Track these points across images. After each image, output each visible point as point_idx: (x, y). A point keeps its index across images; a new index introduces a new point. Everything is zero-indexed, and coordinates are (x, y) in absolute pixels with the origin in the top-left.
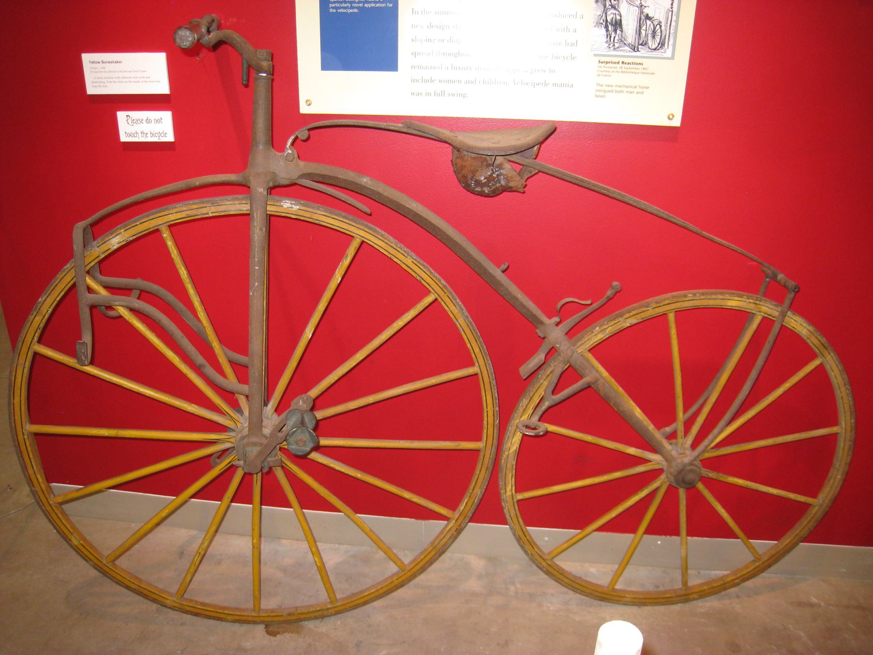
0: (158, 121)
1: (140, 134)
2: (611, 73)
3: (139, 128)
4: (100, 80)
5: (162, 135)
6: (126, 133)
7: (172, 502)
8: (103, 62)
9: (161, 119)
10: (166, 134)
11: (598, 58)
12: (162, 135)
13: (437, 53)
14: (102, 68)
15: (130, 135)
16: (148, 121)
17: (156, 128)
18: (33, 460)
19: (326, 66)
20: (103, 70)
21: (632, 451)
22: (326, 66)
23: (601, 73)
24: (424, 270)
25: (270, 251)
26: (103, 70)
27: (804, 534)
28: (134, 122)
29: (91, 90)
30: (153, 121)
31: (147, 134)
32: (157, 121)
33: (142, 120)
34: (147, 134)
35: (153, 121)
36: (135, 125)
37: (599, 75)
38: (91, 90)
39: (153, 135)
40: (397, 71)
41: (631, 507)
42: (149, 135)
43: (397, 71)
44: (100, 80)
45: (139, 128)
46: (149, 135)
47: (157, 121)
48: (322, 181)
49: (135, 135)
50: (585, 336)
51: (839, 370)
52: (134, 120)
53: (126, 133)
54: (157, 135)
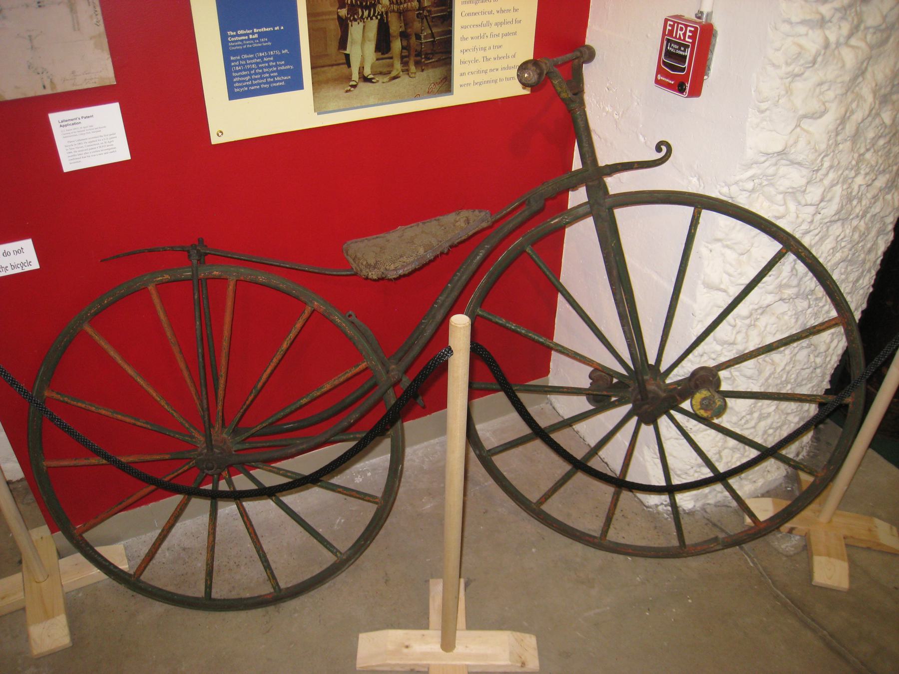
0: (20, 251)
2: (79, 160)
5: (26, 264)
9: (22, 249)
11: (114, 147)
12: (26, 264)
19: (233, 95)
22: (233, 95)
23: (72, 161)
25: (465, 540)
29: (68, 166)
30: (12, 253)
31: (7, 267)
32: (17, 252)
34: (7, 267)
35: (12, 253)
37: (71, 163)
38: (68, 166)
40: (230, 99)
42: (9, 268)
43: (230, 99)
46: (9, 268)
47: (17, 252)
50: (546, 183)
54: (19, 266)
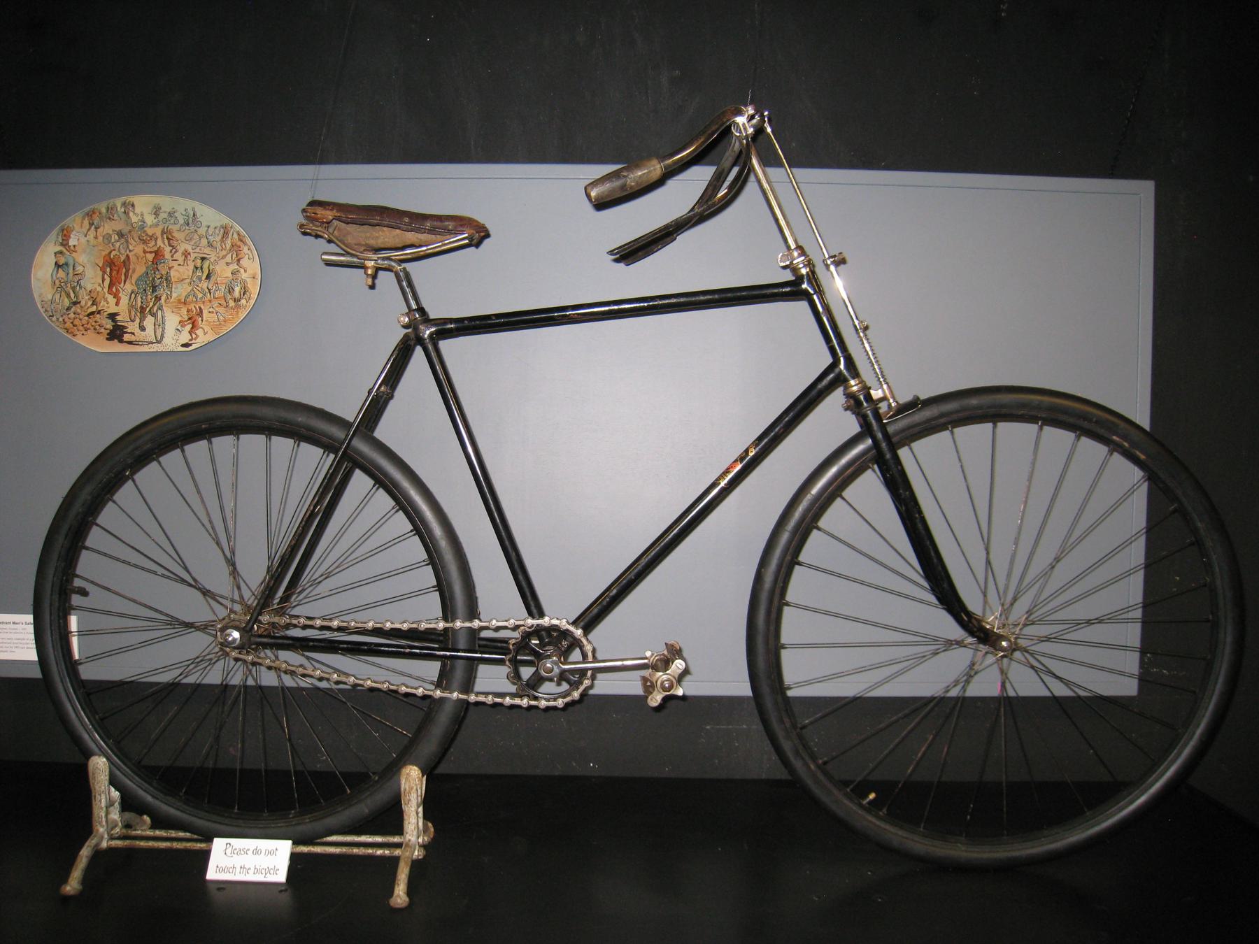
0: (271, 853)
3: (238, 861)
4: (9, 641)
5: (272, 872)
7: (278, 720)
8: (14, 623)
9: (276, 850)
14: (25, 629)
15: (223, 870)
16: (256, 852)
17: (264, 861)
18: (344, 850)
20: (23, 631)
26: (23, 631)
27: (389, 242)
28: (235, 852)
35: (263, 852)
36: (235, 856)
37: (675, 652)
39: (257, 871)
44: (9, 641)
45: (238, 861)
46: (251, 872)
49: (231, 870)
51: (344, 810)
54: (263, 871)
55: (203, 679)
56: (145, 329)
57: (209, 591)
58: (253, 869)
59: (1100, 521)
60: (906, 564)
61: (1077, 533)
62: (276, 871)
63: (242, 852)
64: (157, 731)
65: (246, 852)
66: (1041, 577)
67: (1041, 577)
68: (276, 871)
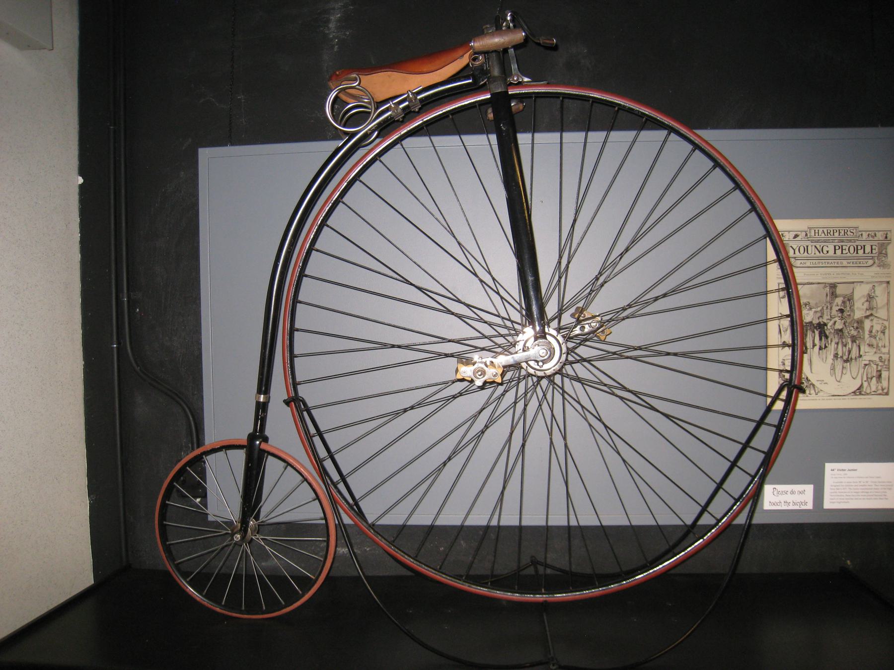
1: (783, 503)
5: (803, 504)
6: (770, 502)
9: (780, 502)
10: (807, 503)
13: (890, 482)
15: (774, 504)
21: (204, 509)
24: (215, 467)
31: (790, 503)
32: (800, 493)
33: (787, 491)
34: (790, 503)
35: (797, 492)
39: (795, 504)
41: (307, 601)
46: (791, 504)
47: (800, 493)
48: (338, 537)
49: (779, 504)
52: (779, 492)
53: (770, 502)
54: (798, 504)
55: (506, 343)
56: (284, 401)
57: (485, 426)
58: (792, 503)
59: (662, 280)
60: (645, 499)
61: (487, 269)
62: (806, 503)
63: (784, 493)
64: (511, 135)
65: (786, 493)
66: (437, 471)
67: (437, 471)
68: (806, 503)
